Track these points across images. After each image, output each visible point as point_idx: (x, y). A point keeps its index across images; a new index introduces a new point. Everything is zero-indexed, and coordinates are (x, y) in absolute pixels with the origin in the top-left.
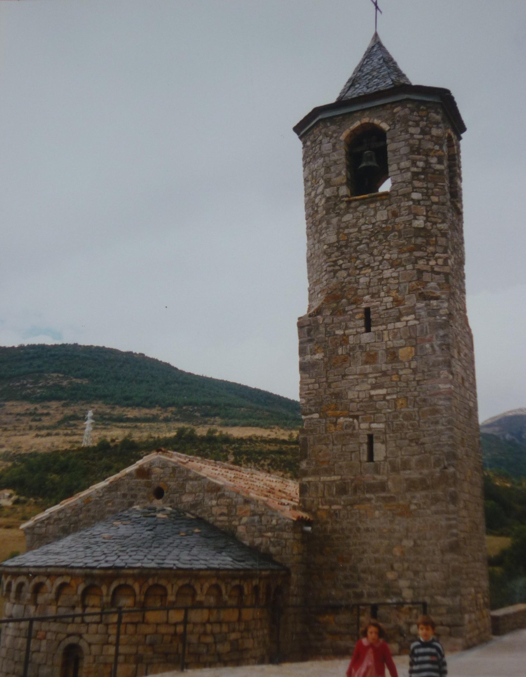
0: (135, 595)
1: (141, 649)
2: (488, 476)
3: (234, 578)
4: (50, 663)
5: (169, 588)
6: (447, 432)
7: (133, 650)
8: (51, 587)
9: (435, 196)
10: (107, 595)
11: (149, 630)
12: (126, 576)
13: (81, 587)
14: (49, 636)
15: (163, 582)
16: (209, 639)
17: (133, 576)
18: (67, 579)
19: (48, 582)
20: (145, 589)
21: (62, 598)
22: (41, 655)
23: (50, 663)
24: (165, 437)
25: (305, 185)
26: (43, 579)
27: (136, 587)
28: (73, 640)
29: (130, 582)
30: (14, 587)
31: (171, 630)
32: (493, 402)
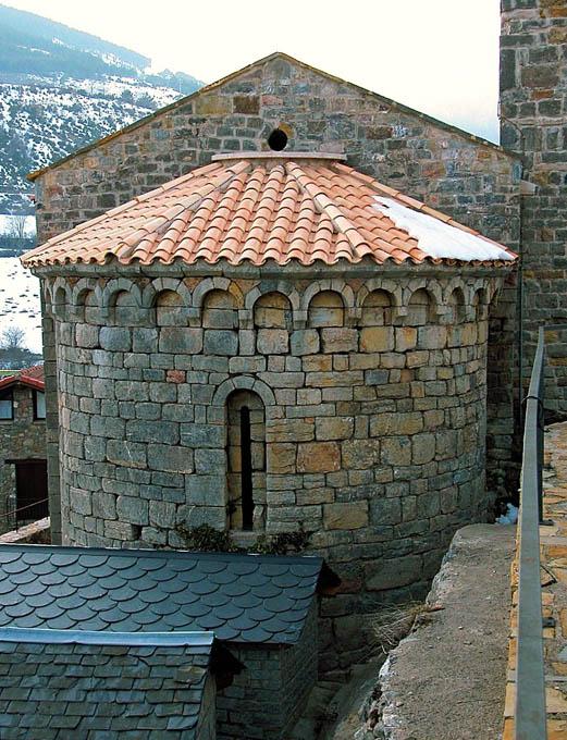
0: (344, 308)
1: (359, 393)
3: (476, 276)
6: (223, 138)
7: (346, 395)
10: (300, 309)
11: (370, 362)
12: (332, 276)
13: (254, 295)
14: (193, 377)
15: (388, 286)
16: (446, 373)
17: (343, 276)
18: (223, 284)
19: (182, 289)
20: (308, 299)
21: (210, 315)
22: (181, 409)
24: (89, 55)
27: (348, 294)
28: (246, 383)
29: (337, 286)
30: (72, 299)
31: (400, 361)
32: (449, 67)
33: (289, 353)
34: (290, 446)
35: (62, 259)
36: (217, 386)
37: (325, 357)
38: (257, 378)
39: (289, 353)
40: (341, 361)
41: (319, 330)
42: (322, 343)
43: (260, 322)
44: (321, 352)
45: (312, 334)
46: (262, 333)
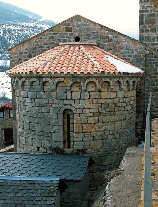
2: (106, 194)
3: (133, 77)
4: (56, 117)
5: (111, 82)
8: (52, 83)
9: (48, 30)
10: (84, 86)
13: (71, 83)
14: (54, 105)
17: (96, 77)
18: (62, 79)
19: (51, 81)
21: (59, 88)
22: (50, 114)
23: (56, 117)
25: (139, 27)
26: (47, 79)
27: (97, 82)
29: (94, 80)
31: (112, 101)
33: (81, 99)
34: (81, 125)
35: (17, 73)
36: (60, 108)
37: (91, 100)
38: (72, 106)
39: (81, 99)
40: (95, 101)
41: (89, 92)
42: (90, 96)
43: (72, 90)
44: (89, 98)
45: (87, 93)
46: (73, 93)
